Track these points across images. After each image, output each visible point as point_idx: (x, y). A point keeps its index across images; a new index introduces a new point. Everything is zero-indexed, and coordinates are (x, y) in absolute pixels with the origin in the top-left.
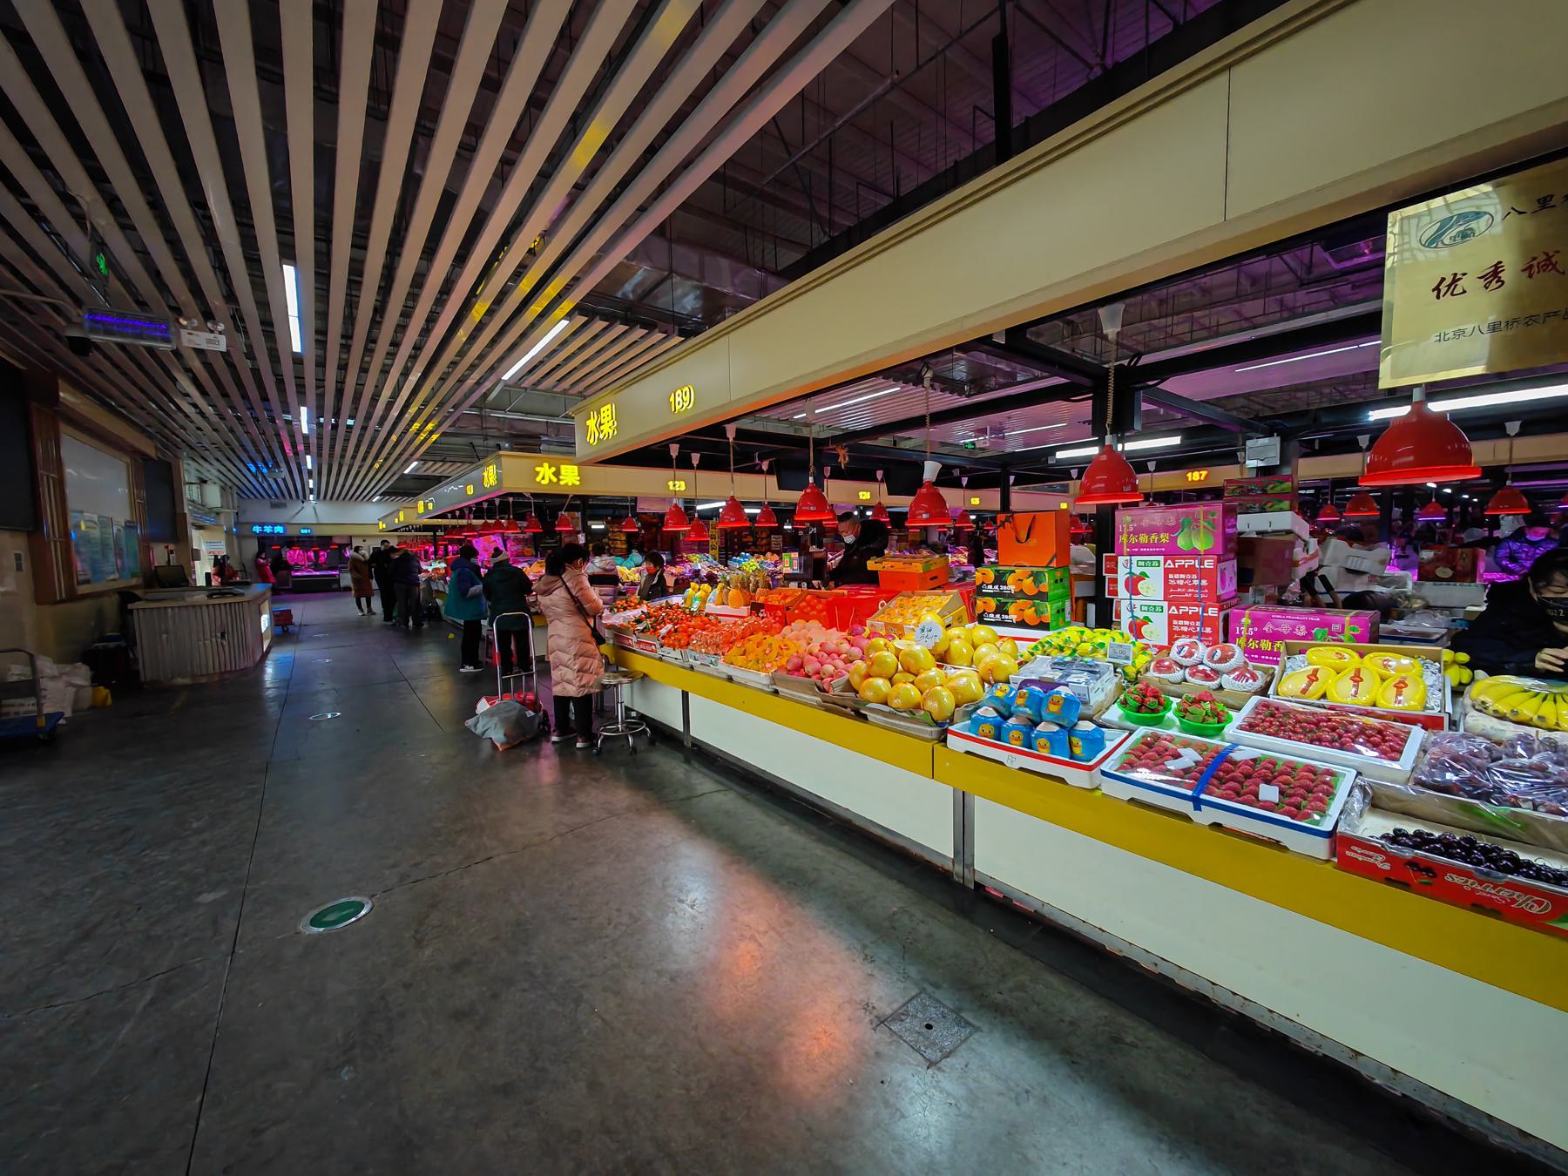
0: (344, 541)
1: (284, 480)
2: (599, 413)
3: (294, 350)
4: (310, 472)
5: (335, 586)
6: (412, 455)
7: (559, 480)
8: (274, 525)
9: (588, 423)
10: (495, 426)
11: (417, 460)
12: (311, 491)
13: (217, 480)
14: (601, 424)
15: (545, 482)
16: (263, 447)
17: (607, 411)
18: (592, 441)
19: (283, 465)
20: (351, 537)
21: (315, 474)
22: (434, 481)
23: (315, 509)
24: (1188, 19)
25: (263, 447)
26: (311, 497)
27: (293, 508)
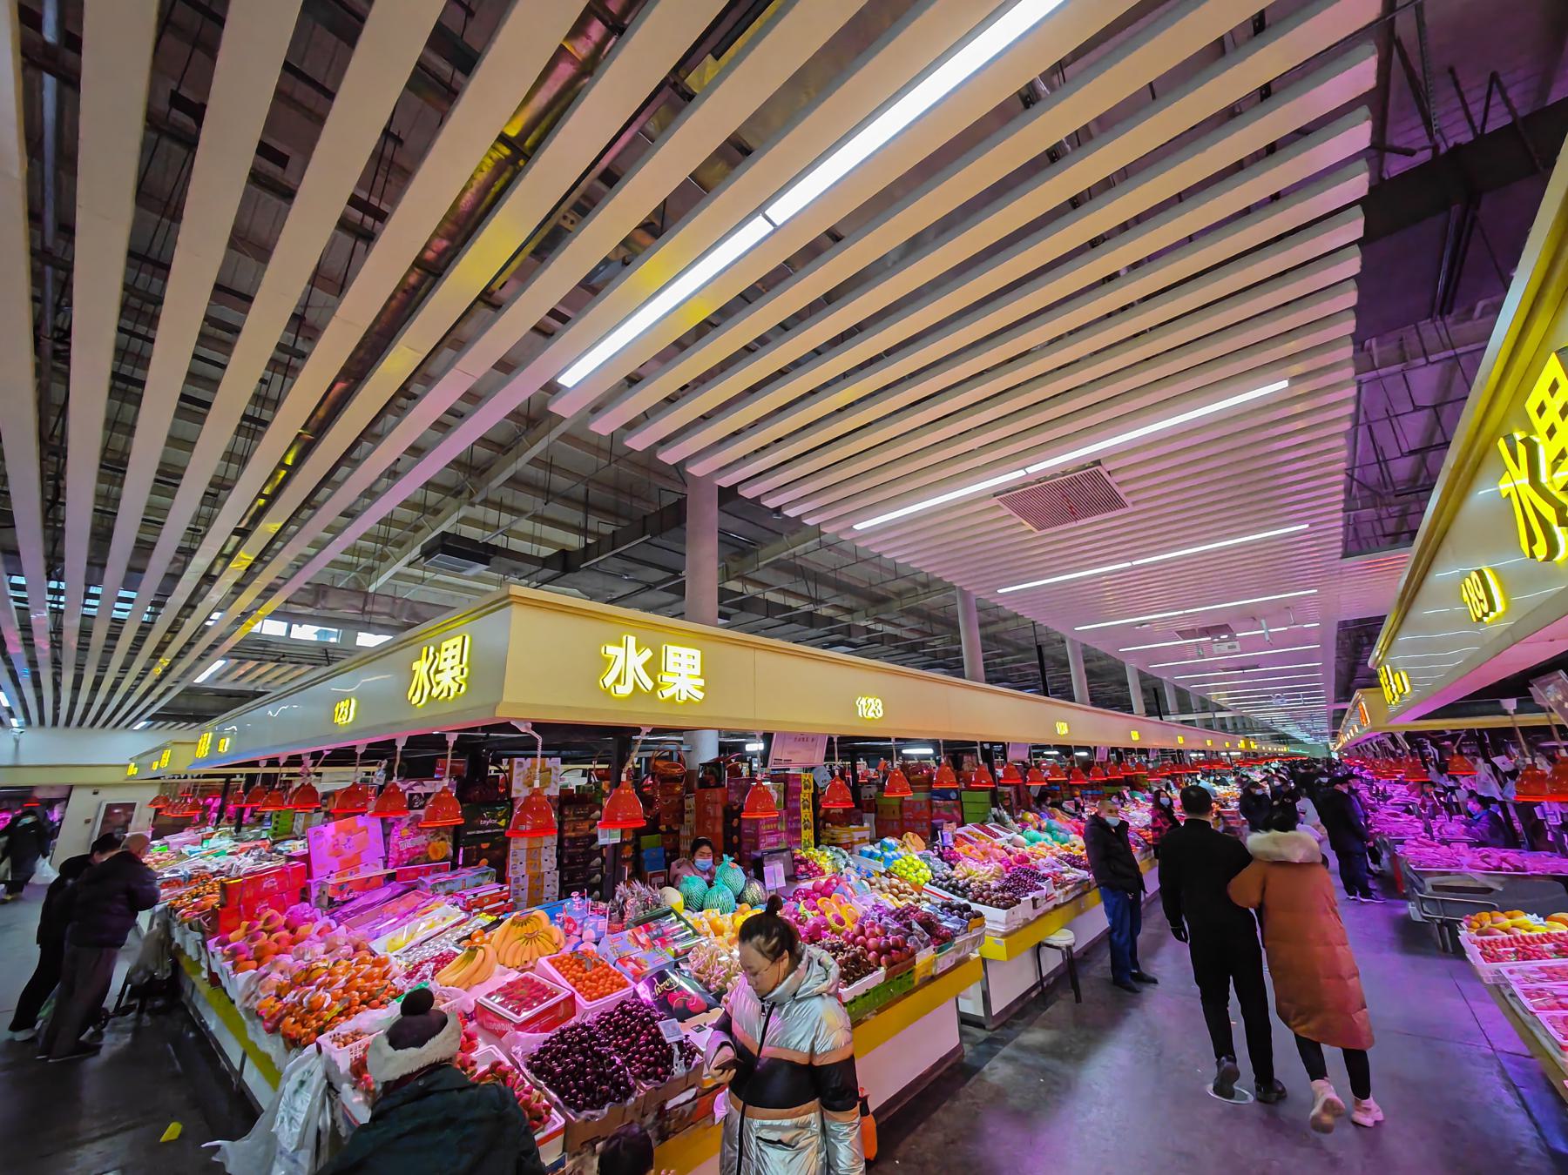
0: (54, 795)
2: (438, 649)
6: (212, 647)
7: (656, 686)
9: (416, 666)
10: (387, 610)
11: (224, 657)
14: (438, 671)
15: (625, 690)
17: (452, 646)
18: (415, 700)
22: (234, 699)
23: (17, 741)
24: (1486, 132)
26: (14, 722)
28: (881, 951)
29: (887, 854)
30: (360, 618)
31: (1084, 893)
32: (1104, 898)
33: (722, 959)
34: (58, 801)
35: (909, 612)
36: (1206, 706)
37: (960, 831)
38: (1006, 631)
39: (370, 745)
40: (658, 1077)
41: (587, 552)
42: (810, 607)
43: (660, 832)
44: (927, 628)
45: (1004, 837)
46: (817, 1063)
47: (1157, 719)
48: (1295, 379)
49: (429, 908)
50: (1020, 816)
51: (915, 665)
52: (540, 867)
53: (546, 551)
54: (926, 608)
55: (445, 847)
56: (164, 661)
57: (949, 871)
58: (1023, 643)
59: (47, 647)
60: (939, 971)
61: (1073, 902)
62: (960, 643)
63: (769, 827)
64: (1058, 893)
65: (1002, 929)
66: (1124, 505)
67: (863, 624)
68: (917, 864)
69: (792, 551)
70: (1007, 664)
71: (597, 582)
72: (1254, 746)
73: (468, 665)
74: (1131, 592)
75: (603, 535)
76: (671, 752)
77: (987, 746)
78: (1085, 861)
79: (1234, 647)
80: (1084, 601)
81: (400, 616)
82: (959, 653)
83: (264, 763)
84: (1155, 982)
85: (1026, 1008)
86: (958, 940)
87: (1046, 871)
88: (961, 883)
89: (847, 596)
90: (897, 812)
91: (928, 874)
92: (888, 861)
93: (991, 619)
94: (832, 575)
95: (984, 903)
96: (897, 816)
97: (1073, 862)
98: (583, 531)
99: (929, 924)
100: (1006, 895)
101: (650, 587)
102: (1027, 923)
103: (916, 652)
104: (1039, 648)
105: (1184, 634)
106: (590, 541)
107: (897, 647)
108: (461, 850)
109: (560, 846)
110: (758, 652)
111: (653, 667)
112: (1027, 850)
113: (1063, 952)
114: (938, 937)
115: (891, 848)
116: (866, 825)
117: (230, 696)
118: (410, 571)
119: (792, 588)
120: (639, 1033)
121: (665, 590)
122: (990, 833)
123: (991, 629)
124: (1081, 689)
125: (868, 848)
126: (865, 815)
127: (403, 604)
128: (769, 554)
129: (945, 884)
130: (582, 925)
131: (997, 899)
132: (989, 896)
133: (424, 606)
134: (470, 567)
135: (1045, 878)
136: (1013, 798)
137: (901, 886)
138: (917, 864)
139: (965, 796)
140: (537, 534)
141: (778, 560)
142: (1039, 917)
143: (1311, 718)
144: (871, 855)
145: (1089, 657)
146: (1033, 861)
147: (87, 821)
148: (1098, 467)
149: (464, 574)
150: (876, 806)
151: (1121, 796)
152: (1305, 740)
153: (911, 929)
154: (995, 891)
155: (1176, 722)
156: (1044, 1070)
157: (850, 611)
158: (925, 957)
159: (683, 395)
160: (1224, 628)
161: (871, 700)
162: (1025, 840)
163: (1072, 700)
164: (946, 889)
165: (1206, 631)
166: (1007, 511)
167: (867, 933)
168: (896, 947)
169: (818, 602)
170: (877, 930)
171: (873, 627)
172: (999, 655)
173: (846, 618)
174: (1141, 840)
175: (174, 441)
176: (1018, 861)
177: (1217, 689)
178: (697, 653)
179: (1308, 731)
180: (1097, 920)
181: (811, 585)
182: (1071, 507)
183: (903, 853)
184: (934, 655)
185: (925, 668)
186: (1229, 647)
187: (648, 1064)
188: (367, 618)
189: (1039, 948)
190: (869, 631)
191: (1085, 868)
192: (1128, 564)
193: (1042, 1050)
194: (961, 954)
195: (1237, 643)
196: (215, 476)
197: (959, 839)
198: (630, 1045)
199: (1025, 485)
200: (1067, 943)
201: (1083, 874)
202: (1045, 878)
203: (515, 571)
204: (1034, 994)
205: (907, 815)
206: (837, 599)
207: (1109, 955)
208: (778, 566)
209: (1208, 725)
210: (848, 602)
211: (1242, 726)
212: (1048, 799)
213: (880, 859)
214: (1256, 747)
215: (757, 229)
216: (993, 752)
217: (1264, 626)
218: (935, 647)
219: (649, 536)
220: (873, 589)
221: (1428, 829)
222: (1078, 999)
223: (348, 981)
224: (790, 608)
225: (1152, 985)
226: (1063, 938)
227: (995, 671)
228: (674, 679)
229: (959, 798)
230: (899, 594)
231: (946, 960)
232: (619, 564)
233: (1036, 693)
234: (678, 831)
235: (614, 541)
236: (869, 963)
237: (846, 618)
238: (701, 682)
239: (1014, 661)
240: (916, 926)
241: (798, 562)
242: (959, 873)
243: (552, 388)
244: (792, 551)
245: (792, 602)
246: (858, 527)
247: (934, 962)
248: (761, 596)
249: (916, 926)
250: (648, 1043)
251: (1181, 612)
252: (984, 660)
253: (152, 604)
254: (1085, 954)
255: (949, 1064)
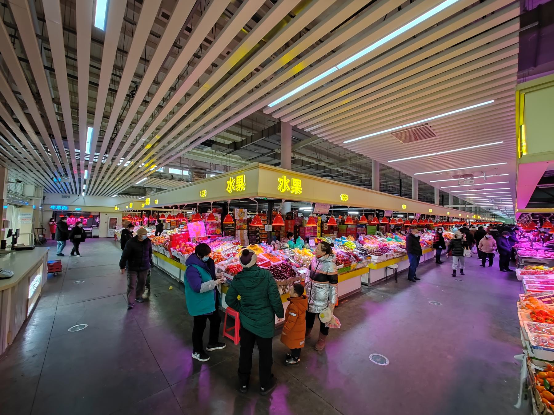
1: (70, 184)
3: (96, 25)
4: (85, 181)
5: (89, 235)
8: (62, 205)
11: (147, 177)
12: (84, 191)
13: (33, 183)
16: (59, 166)
19: (70, 176)
20: (100, 213)
21: (88, 182)
23: (84, 199)
25: (59, 166)
26: (83, 194)
27: (73, 198)
28: (342, 261)
29: (343, 240)
30: (179, 165)
31: (404, 256)
32: (410, 258)
33: (302, 258)
34: (98, 216)
35: (352, 165)
36: (464, 203)
37: (366, 236)
38: (390, 173)
39: (200, 203)
40: (293, 276)
41: (242, 143)
42: (317, 163)
43: (275, 231)
44: (359, 171)
45: (380, 239)
46: (328, 274)
47: (442, 206)
48: (495, 100)
49: (223, 244)
50: (386, 234)
51: (353, 184)
52: (244, 238)
53: (229, 142)
54: (359, 164)
55: (220, 231)
56: (120, 176)
57: (362, 246)
58: (396, 177)
59: (77, 171)
60: (357, 268)
61: (399, 258)
62: (372, 177)
63: (308, 231)
64: (394, 254)
65: (376, 261)
66: (435, 136)
67: (336, 169)
68: (352, 243)
69: (312, 142)
70: (388, 185)
71: (246, 153)
72: (479, 217)
73: (245, 182)
74: (438, 163)
75: (248, 137)
76: (277, 209)
77: (377, 212)
78: (405, 247)
79: (472, 182)
80: (421, 165)
81: (190, 165)
82: (370, 180)
83: (163, 207)
84: (420, 280)
85: (380, 282)
86: (363, 261)
87: (392, 248)
88: (365, 249)
89: (331, 159)
90: (345, 230)
91: (355, 246)
92: (343, 242)
93: (384, 168)
94: (326, 151)
95: (371, 254)
96: (345, 232)
97: (401, 247)
98: (242, 135)
99: (355, 256)
100: (379, 253)
101: (263, 155)
102: (384, 261)
103: (354, 179)
104: (401, 180)
105: (455, 177)
106: (243, 139)
107: (348, 178)
108: (224, 232)
109: (248, 233)
110: (315, 181)
111: (290, 184)
112: (387, 243)
113: (394, 270)
114: (358, 260)
115: (344, 239)
116: (335, 234)
117: (136, 188)
118: (194, 151)
119: (312, 156)
120: (288, 269)
121: (268, 156)
122: (375, 238)
123: (384, 172)
124: (415, 195)
125: (337, 239)
126: (334, 231)
127: (191, 161)
128: (303, 144)
129: (360, 249)
130: (266, 249)
131: (376, 254)
132: (373, 253)
133: (197, 162)
134: (206, 148)
135: (391, 250)
136: (384, 230)
137: (348, 248)
138: (352, 243)
139: (368, 227)
140: (229, 137)
141: (308, 145)
142: (388, 260)
143: (506, 208)
144: (338, 241)
145: (420, 183)
146: (388, 246)
147: (106, 222)
148: (427, 125)
149: (204, 150)
150: (338, 229)
151: (423, 231)
152: (504, 217)
153: (351, 257)
154: (375, 251)
155: (451, 208)
156: (383, 295)
157: (331, 164)
158: (354, 264)
159: (280, 87)
160: (471, 175)
161: (345, 195)
162: (387, 240)
163: (412, 198)
164: (360, 250)
165: (464, 176)
166: (395, 138)
167: (339, 256)
168: (347, 260)
169: (320, 161)
170: (342, 256)
171: (339, 170)
172: (386, 182)
173: (330, 167)
174: (426, 243)
175: (90, 98)
176: (383, 245)
177: (469, 196)
178: (300, 181)
179: (504, 213)
180: (406, 265)
181: (318, 154)
182: (416, 136)
183: (347, 241)
184: (361, 181)
185: (357, 185)
186: (470, 182)
187: (291, 274)
188: (182, 165)
189: (386, 268)
190: (338, 171)
191: (405, 249)
192: (435, 154)
193: (384, 291)
194: (364, 265)
195: (473, 181)
196: (133, 119)
197: (365, 239)
198: (286, 270)
199: (402, 130)
200: (395, 267)
201: (404, 250)
202: (391, 250)
203: (219, 149)
204: (383, 280)
205: (348, 232)
206: (327, 160)
207: (408, 274)
208: (307, 147)
209: (464, 210)
210: (331, 160)
211: (479, 210)
212: (397, 229)
213: (341, 242)
214: (480, 218)
215: (334, 69)
216: (380, 213)
217: (485, 175)
218: (361, 178)
219: (264, 138)
220: (341, 156)
221: (532, 245)
222: (396, 282)
223: (214, 256)
224: (310, 163)
225: (419, 281)
226: (394, 266)
227: (383, 187)
228: (295, 188)
229: (366, 227)
230: (350, 158)
231: (360, 265)
232: (254, 147)
233: (398, 195)
234: (279, 232)
235: (252, 139)
236: (339, 263)
237: (330, 167)
238: (301, 189)
239: (391, 184)
240: (352, 256)
241: (314, 146)
242: (365, 247)
243: (266, 107)
244: (312, 142)
245: (310, 160)
246: (345, 142)
247: (356, 266)
248: (300, 158)
249: (352, 256)
250: (290, 270)
251: (454, 169)
252: (380, 183)
253: (111, 161)
254: (401, 273)
255: (357, 292)
